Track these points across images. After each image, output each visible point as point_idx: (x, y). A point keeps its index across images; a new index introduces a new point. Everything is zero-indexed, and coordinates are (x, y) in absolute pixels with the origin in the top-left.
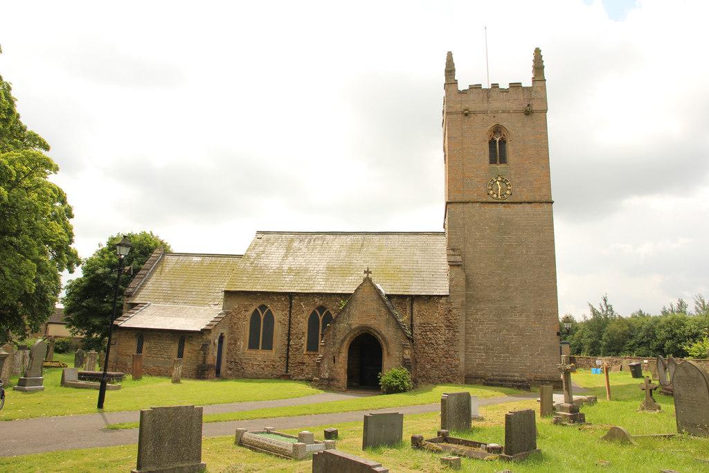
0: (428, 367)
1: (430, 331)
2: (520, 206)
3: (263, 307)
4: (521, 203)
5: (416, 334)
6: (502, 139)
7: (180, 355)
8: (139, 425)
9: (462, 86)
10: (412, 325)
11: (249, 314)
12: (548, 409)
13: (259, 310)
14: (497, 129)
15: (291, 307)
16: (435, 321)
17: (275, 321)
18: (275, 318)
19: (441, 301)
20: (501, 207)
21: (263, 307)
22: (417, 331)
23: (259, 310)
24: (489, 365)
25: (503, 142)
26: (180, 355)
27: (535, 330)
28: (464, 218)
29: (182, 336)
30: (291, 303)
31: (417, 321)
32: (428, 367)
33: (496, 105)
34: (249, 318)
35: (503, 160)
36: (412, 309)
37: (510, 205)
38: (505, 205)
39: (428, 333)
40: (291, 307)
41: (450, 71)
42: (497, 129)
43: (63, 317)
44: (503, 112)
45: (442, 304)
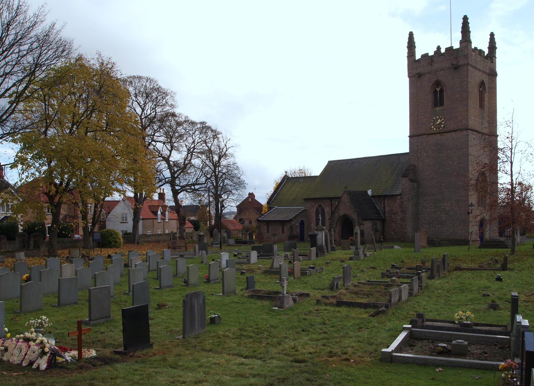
0: (393, 234)
1: (393, 214)
2: (449, 134)
3: (320, 206)
4: (449, 132)
5: (387, 216)
6: (441, 88)
7: (283, 232)
8: (88, 306)
9: (418, 56)
10: (385, 212)
11: (315, 209)
12: (352, 281)
13: (318, 207)
14: (438, 83)
15: (332, 205)
16: (395, 209)
17: (326, 212)
18: (326, 211)
19: (398, 198)
20: (438, 135)
21: (320, 206)
22: (387, 215)
23: (318, 207)
24: (430, 232)
25: (442, 91)
26: (283, 232)
27: (455, 211)
28: (417, 146)
29: (282, 223)
30: (332, 203)
31: (387, 209)
32: (393, 234)
33: (436, 66)
34: (315, 211)
35: (442, 104)
36: (384, 203)
37: (443, 134)
38: (441, 134)
39: (392, 215)
40: (332, 205)
41: (411, 45)
42: (438, 83)
43: (145, 233)
44: (441, 70)
45: (399, 199)
